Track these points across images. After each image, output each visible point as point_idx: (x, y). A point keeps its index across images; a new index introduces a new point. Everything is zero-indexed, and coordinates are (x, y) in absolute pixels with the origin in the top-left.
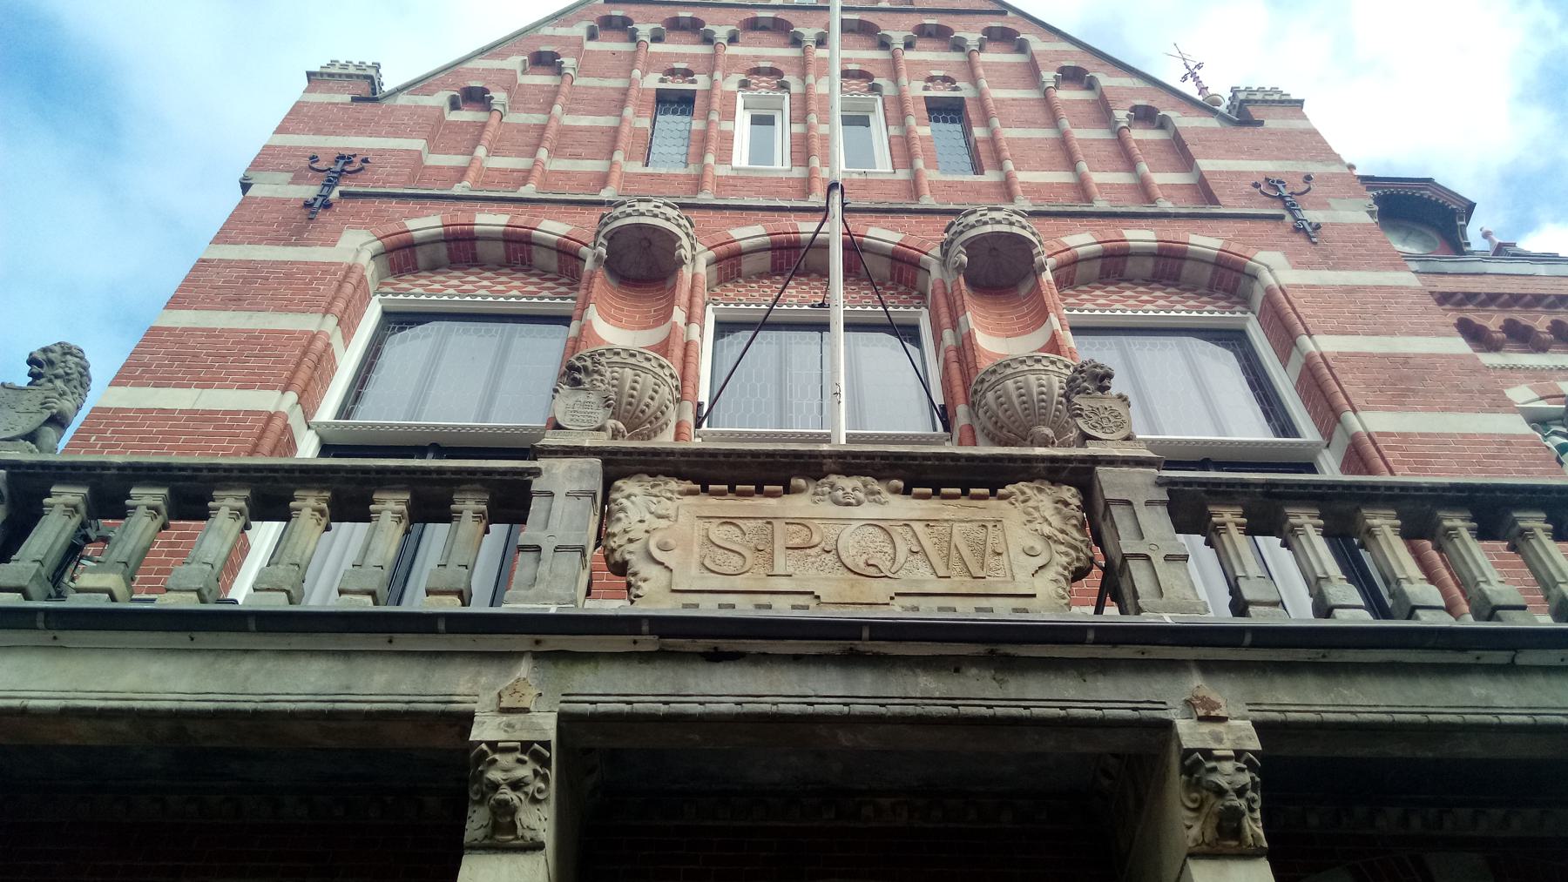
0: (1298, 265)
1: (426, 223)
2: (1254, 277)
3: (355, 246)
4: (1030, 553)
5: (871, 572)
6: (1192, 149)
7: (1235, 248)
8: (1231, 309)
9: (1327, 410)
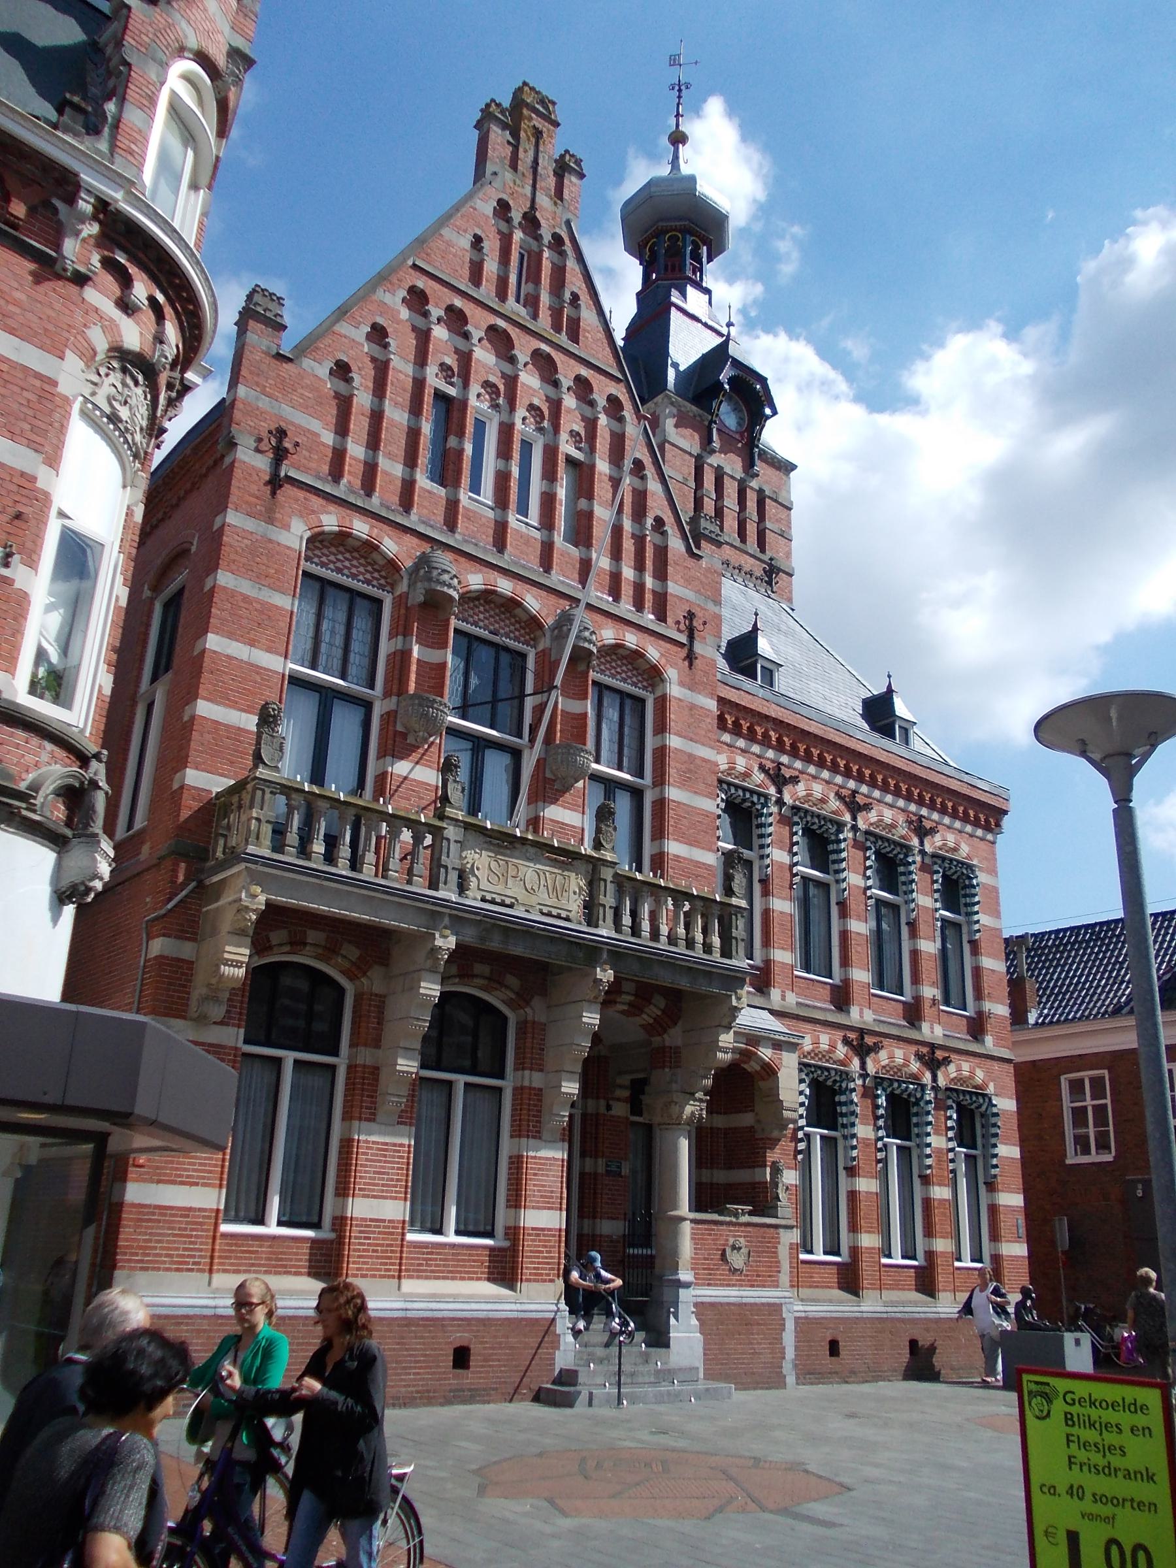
0: (681, 684)
1: (330, 521)
2: (663, 681)
3: (294, 535)
4: (575, 893)
5: (530, 891)
6: (670, 569)
7: (663, 662)
8: (645, 688)
9: (660, 780)
